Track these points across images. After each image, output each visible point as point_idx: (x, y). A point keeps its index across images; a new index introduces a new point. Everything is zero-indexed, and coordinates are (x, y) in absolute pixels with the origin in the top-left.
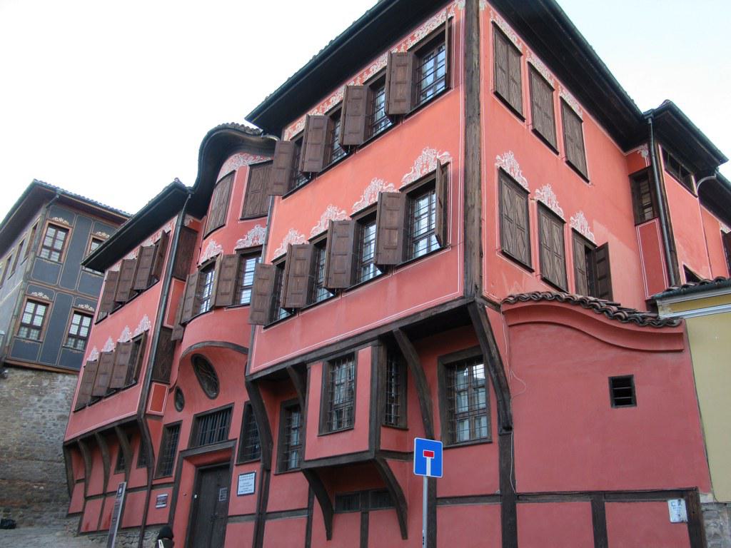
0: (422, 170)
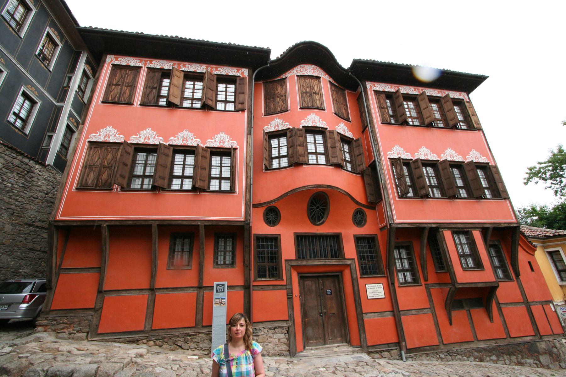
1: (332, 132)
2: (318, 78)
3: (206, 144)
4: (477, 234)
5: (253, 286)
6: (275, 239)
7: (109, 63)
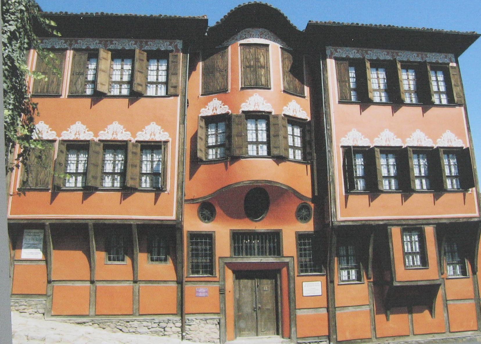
0: (213, 110)
1: (276, 117)
2: (267, 46)
4: (429, 231)
5: (186, 281)
6: (209, 237)
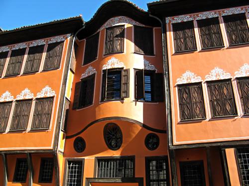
3: (235, 75)
7: (169, 24)
